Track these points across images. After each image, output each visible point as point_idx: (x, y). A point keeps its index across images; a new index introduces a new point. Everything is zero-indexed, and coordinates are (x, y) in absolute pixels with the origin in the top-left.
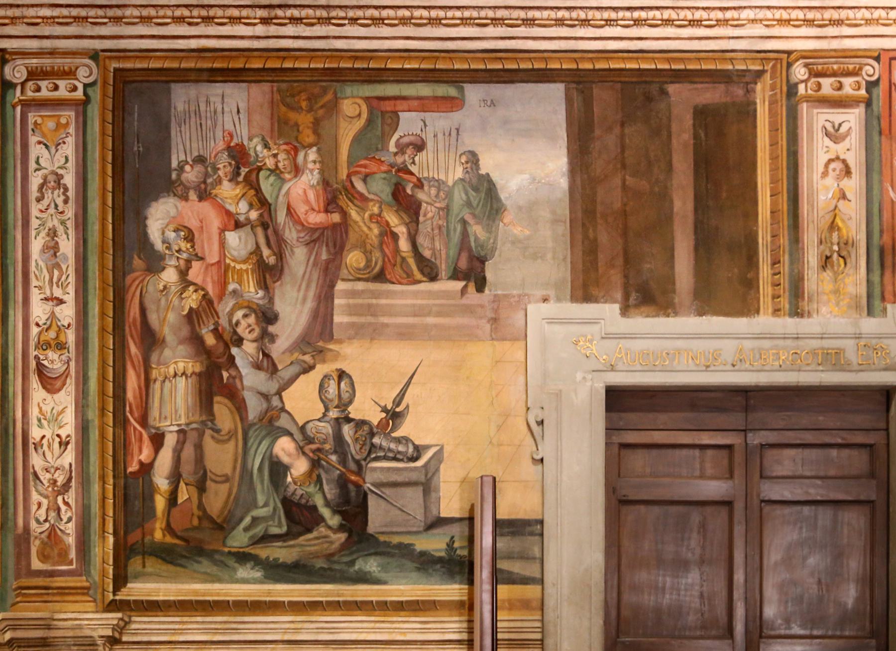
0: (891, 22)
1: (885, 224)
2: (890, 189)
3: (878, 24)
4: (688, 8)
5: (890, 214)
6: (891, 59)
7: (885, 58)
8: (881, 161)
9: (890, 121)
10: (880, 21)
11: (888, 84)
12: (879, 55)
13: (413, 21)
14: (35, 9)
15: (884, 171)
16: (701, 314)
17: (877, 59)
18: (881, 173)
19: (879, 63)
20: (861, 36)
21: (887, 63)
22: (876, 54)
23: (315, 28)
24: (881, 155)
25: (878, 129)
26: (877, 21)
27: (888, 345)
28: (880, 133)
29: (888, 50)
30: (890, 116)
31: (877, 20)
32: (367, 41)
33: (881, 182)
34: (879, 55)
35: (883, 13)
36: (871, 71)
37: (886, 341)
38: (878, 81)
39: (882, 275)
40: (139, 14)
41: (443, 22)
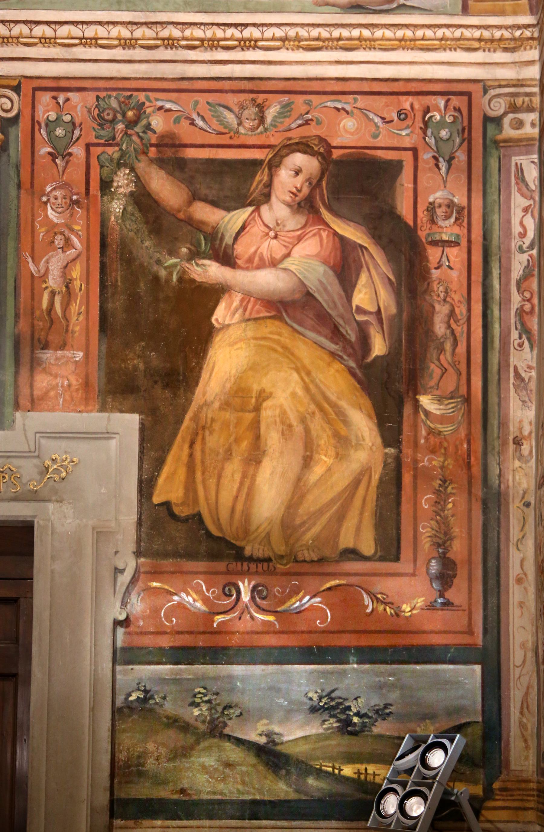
0: (36, 40)
1: (22, 306)
2: (30, 260)
3: (18, 43)
4: (25, 22)
5: (29, 293)
6: (35, 89)
7: (27, 88)
8: (18, 224)
9: (33, 171)
10: (21, 40)
11: (30, 123)
12: (20, 83)
13: (21, 40)
14: (470, 30)
15: (23, 237)
16: (103, 409)
17: (17, 89)
18: (18, 239)
19: (19, 95)
20: (443, 63)
21: (30, 94)
22: (15, 83)
23: (74, 49)
24: (18, 216)
25: (16, 181)
26: (17, 40)
27: (18, 467)
28: (19, 186)
29: (31, 78)
30: (33, 163)
31: (17, 38)
32: (264, 67)
33: (18, 250)
34: (20, 83)
35: (25, 29)
36: (8, 105)
37: (16, 462)
38: (17, 117)
39: (17, 373)
40: (80, 34)
41: (260, 43)
